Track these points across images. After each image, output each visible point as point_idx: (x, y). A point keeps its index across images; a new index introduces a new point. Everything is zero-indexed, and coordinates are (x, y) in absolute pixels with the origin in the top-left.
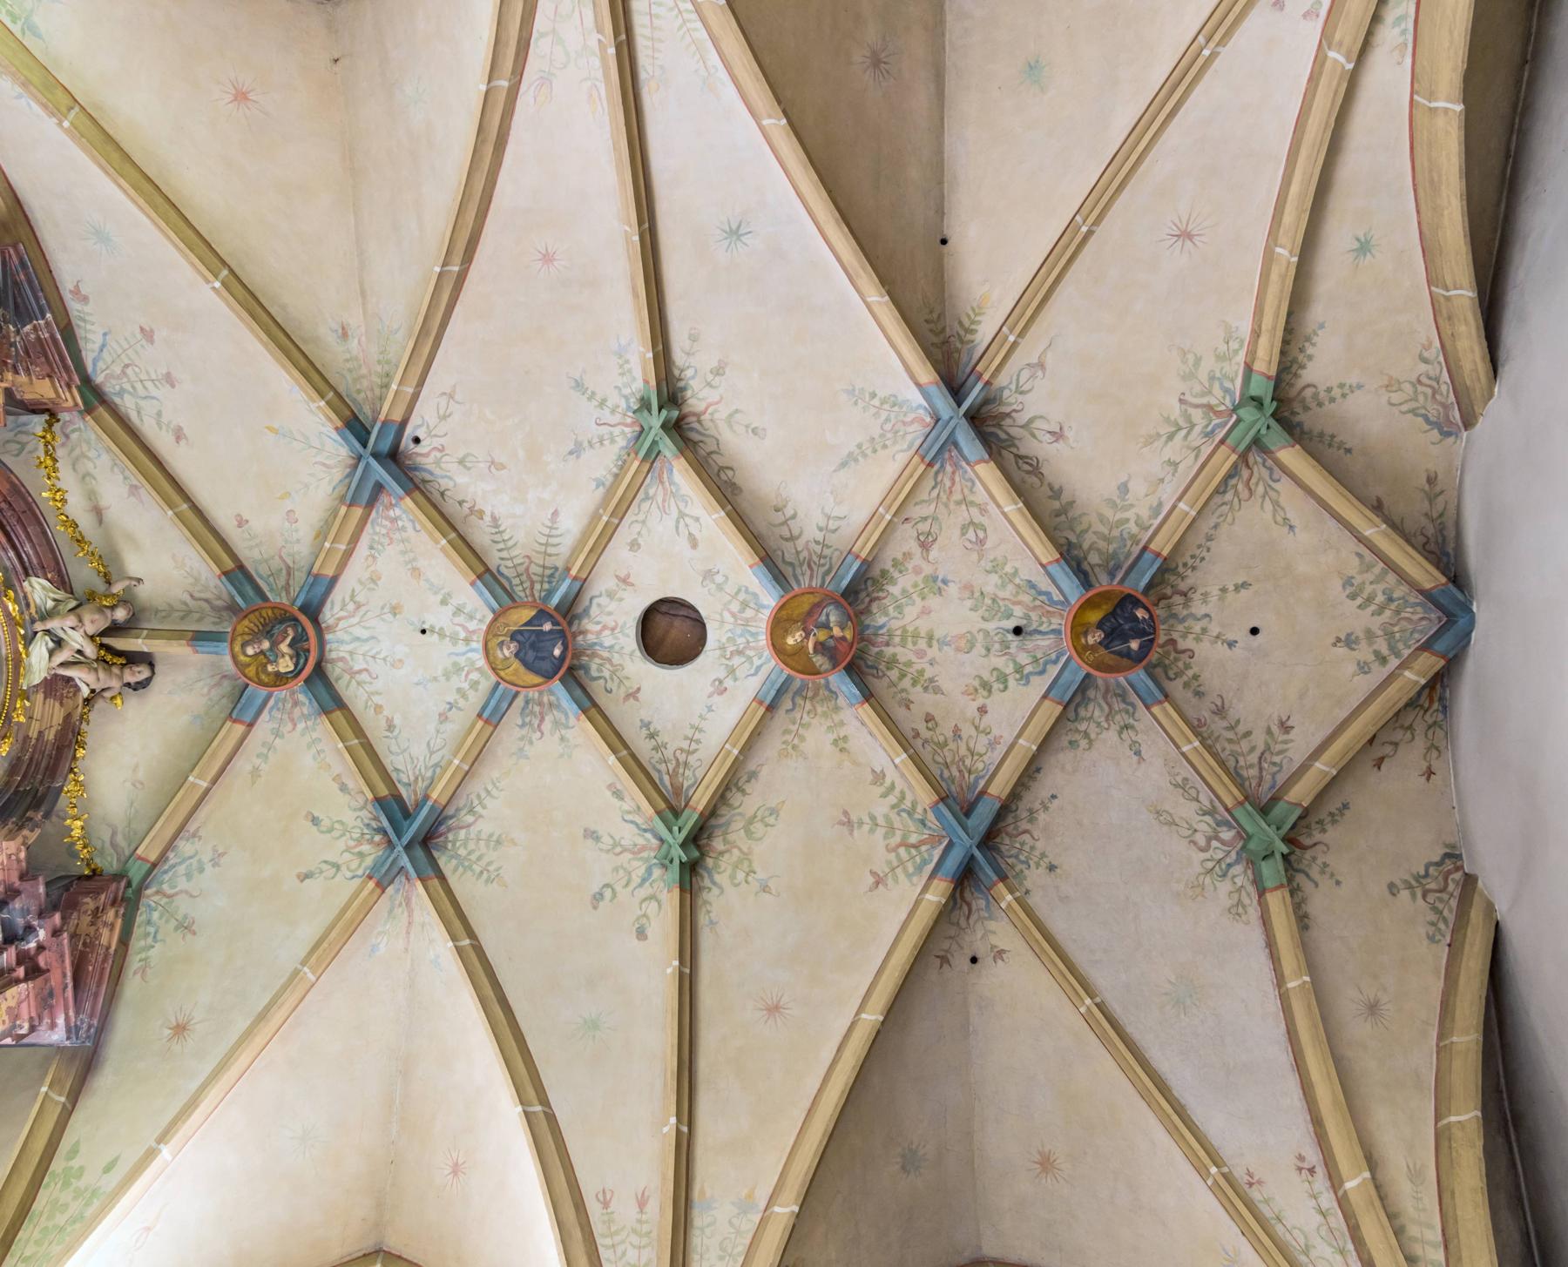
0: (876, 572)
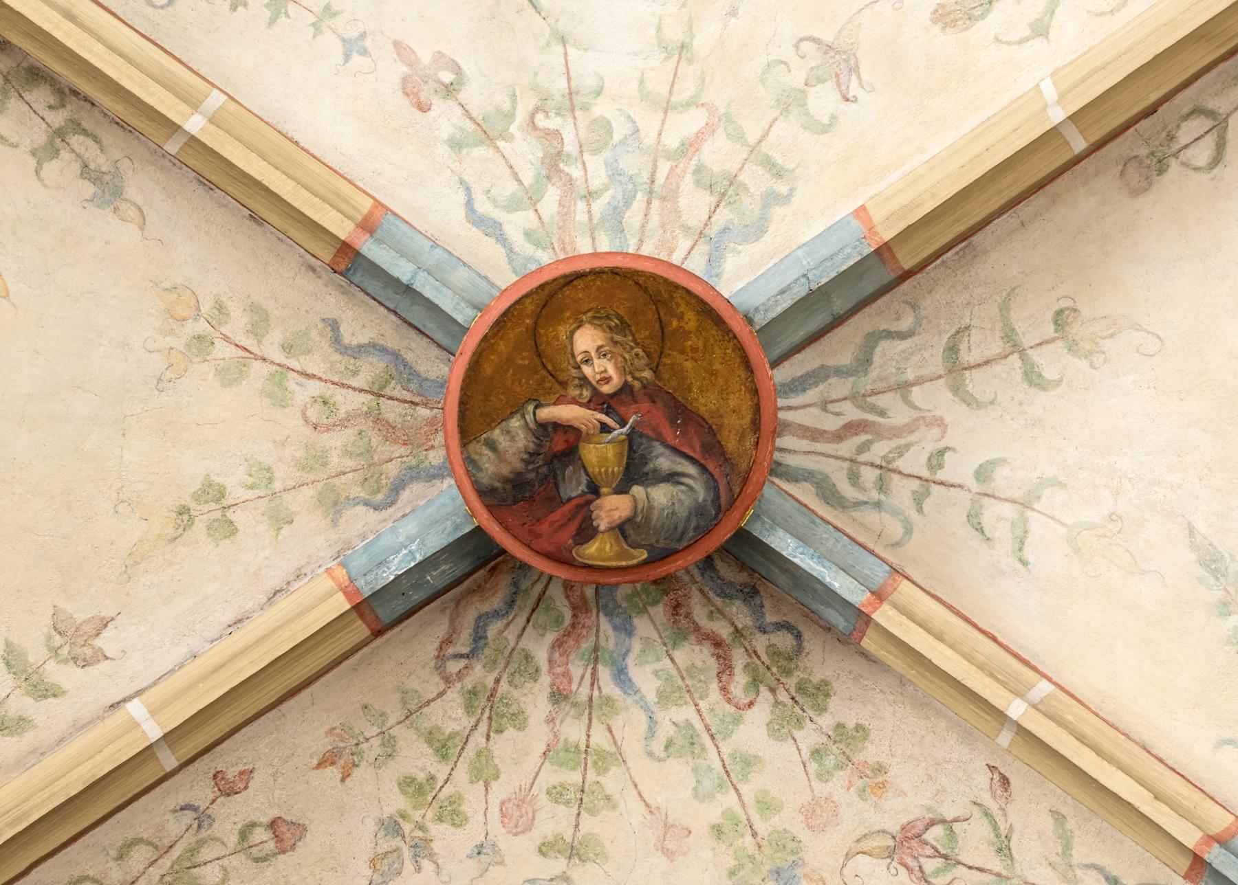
0: (821, 662)
